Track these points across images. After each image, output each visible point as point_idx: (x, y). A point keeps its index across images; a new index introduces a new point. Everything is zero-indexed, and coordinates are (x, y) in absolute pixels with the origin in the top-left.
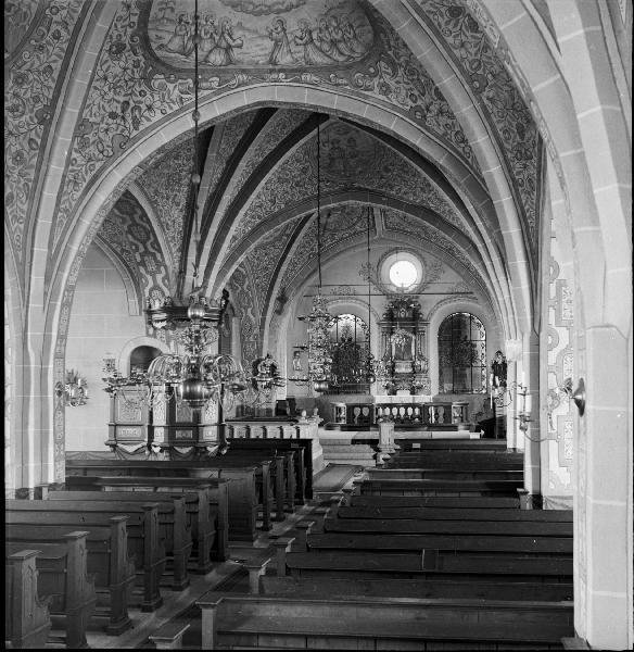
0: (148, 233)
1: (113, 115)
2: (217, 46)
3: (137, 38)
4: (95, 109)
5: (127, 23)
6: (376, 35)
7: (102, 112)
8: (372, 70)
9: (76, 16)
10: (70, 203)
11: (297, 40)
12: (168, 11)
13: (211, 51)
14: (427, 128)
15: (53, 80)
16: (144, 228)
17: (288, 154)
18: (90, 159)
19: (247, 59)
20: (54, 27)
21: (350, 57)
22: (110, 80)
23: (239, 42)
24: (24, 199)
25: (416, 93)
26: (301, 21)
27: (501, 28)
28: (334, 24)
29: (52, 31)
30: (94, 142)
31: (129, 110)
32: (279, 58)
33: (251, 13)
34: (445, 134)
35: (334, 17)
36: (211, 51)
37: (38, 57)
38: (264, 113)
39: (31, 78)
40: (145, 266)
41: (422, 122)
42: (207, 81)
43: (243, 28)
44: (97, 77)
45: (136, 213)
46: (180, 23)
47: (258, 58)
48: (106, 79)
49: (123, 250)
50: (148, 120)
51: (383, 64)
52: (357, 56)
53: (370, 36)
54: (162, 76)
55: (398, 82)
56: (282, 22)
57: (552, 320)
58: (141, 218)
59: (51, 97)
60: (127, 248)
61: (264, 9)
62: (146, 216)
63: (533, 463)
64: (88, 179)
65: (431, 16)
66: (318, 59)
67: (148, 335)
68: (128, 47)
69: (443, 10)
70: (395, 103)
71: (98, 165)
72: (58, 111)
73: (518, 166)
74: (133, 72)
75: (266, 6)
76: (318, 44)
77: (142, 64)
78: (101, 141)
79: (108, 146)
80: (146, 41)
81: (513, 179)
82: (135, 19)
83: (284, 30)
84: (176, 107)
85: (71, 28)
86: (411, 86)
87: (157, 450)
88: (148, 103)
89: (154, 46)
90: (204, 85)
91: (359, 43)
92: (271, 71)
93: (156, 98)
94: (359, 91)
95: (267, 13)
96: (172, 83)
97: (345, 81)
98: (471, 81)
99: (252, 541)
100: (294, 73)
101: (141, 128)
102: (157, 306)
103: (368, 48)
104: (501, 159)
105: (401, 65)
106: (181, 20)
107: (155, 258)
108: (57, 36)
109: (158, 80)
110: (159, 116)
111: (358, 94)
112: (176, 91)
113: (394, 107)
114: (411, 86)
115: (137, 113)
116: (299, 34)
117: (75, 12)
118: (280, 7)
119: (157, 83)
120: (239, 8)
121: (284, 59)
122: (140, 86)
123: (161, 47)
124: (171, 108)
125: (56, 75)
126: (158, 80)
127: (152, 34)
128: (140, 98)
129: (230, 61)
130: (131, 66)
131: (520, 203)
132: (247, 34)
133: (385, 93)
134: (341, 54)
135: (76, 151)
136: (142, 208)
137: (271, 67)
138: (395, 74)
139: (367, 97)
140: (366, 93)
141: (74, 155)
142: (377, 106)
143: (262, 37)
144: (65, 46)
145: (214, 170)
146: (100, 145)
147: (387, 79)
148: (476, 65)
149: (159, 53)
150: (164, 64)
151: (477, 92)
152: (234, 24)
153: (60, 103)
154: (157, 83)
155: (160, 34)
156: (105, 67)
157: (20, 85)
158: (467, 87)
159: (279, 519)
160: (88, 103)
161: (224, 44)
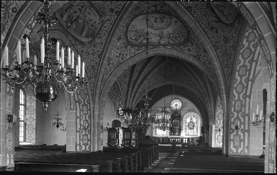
0: (118, 90)
1: (117, 56)
2: (145, 38)
3: (125, 36)
4: (113, 55)
5: (123, 31)
6: (188, 36)
7: (114, 55)
9: (110, 29)
10: (105, 80)
12: (133, 28)
13: (143, 40)
14: (200, 61)
15: (103, 46)
16: (117, 89)
17: (155, 71)
18: (110, 68)
20: (104, 32)
22: (117, 47)
23: (150, 37)
24: (94, 78)
25: (198, 51)
26: (168, 32)
27: (256, 19)
29: (103, 33)
30: (112, 63)
34: (205, 62)
36: (143, 40)
37: (99, 40)
38: (134, 67)
39: (97, 45)
40: (117, 99)
41: (199, 59)
42: (142, 48)
43: (152, 34)
44: (114, 46)
45: (115, 85)
48: (116, 46)
49: (111, 95)
51: (189, 43)
53: (187, 35)
54: (130, 46)
55: (193, 48)
56: (162, 32)
57: (233, 111)
58: (117, 86)
59: (102, 51)
60: (112, 94)
61: (158, 28)
62: (118, 86)
63: (226, 147)
64: (110, 73)
65: (205, 30)
66: (171, 42)
67: (117, 117)
69: (209, 27)
70: (192, 54)
71: (112, 70)
72: (103, 54)
73: (226, 70)
75: (158, 27)
76: (172, 38)
78: (114, 63)
79: (115, 65)
80: (127, 36)
81: (224, 74)
82: (124, 30)
83: (163, 34)
84: (133, 55)
85: (108, 32)
86: (197, 49)
87: (120, 146)
89: (129, 38)
91: (183, 37)
92: (159, 45)
93: (128, 52)
95: (159, 29)
96: (133, 48)
98: (214, 47)
99: (148, 167)
101: (124, 60)
102: (120, 109)
104: (221, 68)
106: (136, 31)
107: (120, 97)
108: (105, 35)
109: (129, 47)
110: (128, 57)
111: (181, 52)
112: (134, 51)
113: (191, 55)
114: (197, 49)
115: (123, 56)
116: (167, 35)
117: (110, 28)
118: (162, 28)
121: (162, 42)
123: (131, 38)
124: (132, 55)
125: (103, 45)
126: (129, 47)
127: (128, 35)
129: (148, 42)
131: (225, 80)
132: (153, 35)
133: (188, 51)
134: (178, 40)
135: (107, 66)
136: (117, 84)
137: (159, 44)
139: (184, 52)
140: (184, 51)
141: (107, 67)
142: (185, 54)
144: (106, 37)
145: (135, 75)
146: (113, 64)
147: (190, 47)
148: (216, 42)
149: (130, 40)
150: (131, 43)
151: (216, 50)
153: (104, 53)
156: (116, 43)
157: (94, 47)
158: (213, 49)
159: (153, 163)
160: (111, 53)
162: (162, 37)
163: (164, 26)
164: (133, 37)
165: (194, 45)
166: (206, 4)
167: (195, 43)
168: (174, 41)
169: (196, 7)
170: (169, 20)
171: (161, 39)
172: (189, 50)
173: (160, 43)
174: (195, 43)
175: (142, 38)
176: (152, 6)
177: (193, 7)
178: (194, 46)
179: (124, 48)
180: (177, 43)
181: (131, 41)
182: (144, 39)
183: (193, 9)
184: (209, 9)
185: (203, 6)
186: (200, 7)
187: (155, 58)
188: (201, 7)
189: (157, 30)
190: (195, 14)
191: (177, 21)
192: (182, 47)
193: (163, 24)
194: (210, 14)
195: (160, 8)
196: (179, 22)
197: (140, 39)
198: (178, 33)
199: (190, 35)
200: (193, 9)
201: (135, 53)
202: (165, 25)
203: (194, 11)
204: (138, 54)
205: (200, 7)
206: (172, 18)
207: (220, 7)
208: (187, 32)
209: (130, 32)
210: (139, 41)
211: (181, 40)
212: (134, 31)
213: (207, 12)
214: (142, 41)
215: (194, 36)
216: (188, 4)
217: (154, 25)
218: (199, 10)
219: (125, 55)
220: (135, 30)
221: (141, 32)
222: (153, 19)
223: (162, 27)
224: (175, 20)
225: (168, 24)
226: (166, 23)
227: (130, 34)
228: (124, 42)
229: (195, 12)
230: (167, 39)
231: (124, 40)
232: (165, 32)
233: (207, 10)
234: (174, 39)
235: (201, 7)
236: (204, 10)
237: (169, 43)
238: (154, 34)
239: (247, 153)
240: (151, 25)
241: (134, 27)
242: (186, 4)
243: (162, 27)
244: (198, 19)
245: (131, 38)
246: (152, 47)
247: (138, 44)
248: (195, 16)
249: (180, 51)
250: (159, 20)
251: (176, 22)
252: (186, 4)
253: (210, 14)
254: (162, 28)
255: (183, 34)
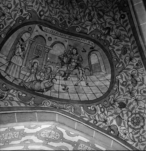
166: (24, 17)
184: (14, 22)
185: (21, 11)
186: (21, 5)
187: (136, 142)
188: (19, 6)
194: (5, 27)
205: (21, 5)
207: (21, 45)
213: (9, 19)
233: (12, 20)
235: (19, 6)
236: (13, 13)
239: (145, 97)
253: (5, 27)
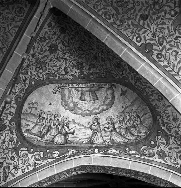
2: (60, 133)
3: (13, 123)
6: (154, 118)
8: (153, 143)
11: (106, 129)
12: (34, 109)
13: (56, 136)
19: (76, 140)
21: (138, 136)
23: (72, 131)
28: (128, 117)
31: (3, 167)
32: (95, 140)
33: (80, 114)
35: (128, 113)
36: (56, 136)
42: (51, 153)
43: (75, 123)
46: (40, 117)
47: (83, 140)
50: (13, 175)
52: (143, 135)
53: (150, 120)
54: (26, 149)
55: (170, 149)
56: (97, 120)
66: (119, 140)
68: (8, 128)
70: (169, 163)
74: (9, 144)
75: (88, 111)
76: (118, 130)
77: (15, 140)
80: (19, 126)
83: (99, 124)
84: (31, 169)
88: (15, 164)
90: (49, 155)
93: (20, 162)
94: (145, 158)
95: (89, 115)
97: (135, 152)
100: (104, 148)
101: (8, 180)
103: (149, 128)
105: (172, 135)
109: (24, 151)
110: (20, 173)
111: (145, 160)
112: (33, 159)
113: (169, 167)
115: (7, 170)
116: (107, 126)
118: (97, 111)
119: (22, 153)
120: (43, 13)
121: (98, 141)
122: (12, 153)
124: (28, 169)
126: (24, 151)
127: (23, 122)
128: (10, 161)
129: (66, 142)
130: (8, 140)
132: (77, 126)
133: (162, 158)
137: (90, 145)
138: (168, 141)
139: (150, 161)
143: (85, 128)
147: (162, 147)
149: (26, 135)
150: (28, 142)
152: (70, 120)
154: (22, 153)
155: (27, 123)
161: (64, 131)
162: (97, 130)
163: (99, 107)
164: (33, 128)
165: (172, 140)
167: (174, 134)
168: (124, 137)
169: (161, 45)
170: (109, 92)
171: (94, 133)
172: (162, 155)
173: (93, 143)
174: (174, 134)
175: (54, 132)
176: (73, 67)
177: (154, 44)
178: (171, 142)
179: (10, 152)
180: (130, 140)
181: (28, 137)
182: (58, 134)
183: (155, 50)
186: (171, 41)
188: (172, 43)
189: (84, 115)
190: (162, 59)
191: (126, 91)
192: (144, 149)
193: (98, 103)
195: (89, 69)
196: (131, 91)
197: (49, 135)
198: (130, 119)
199: (158, 117)
200: (155, 50)
201: (35, 166)
202: (103, 105)
203: (158, 54)
204: (44, 166)
205: (171, 41)
206: (113, 87)
208: (151, 110)
209: (26, 115)
210: (47, 138)
211: (139, 132)
212: (35, 115)
214: (53, 139)
215: (169, 116)
216: (143, 38)
217: (79, 106)
218: (169, 49)
219: (12, 167)
220: (37, 113)
221: (51, 119)
222: (76, 95)
223: (96, 109)
224: (122, 90)
225: (107, 102)
226: (104, 102)
227: (27, 120)
228: (13, 138)
229: (162, 56)
230: (108, 134)
231: (12, 133)
232: (104, 120)
234: (123, 132)
237: (113, 142)
238: (78, 124)
240: (72, 105)
241: (35, 106)
242: (139, 39)
243: (96, 109)
244: (171, 71)
245: (28, 130)
246: (74, 151)
247: (44, 145)
248: (162, 64)
249: (141, 159)
250: (87, 97)
251: (123, 93)
252: (139, 39)
254: (97, 111)
255: (142, 119)
